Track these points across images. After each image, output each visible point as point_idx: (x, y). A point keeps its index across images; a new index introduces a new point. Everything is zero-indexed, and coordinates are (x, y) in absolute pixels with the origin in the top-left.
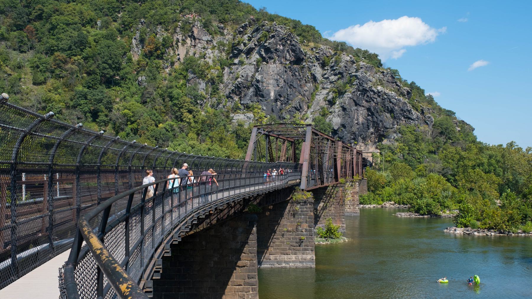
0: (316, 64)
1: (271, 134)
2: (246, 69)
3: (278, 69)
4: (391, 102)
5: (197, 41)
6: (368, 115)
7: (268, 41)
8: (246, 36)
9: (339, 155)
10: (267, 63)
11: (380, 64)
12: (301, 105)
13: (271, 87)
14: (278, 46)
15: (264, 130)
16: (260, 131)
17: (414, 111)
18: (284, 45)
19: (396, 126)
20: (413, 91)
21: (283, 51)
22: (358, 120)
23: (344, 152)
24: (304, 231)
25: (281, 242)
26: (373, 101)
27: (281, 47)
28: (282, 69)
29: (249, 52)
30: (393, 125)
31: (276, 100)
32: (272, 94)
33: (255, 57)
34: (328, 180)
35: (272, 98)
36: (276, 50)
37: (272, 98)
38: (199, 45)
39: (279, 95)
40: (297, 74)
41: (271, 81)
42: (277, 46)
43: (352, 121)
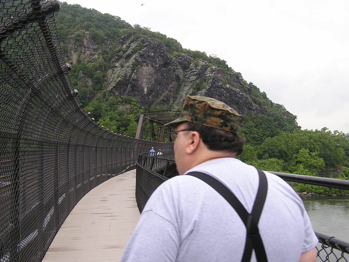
21: (153, 57)
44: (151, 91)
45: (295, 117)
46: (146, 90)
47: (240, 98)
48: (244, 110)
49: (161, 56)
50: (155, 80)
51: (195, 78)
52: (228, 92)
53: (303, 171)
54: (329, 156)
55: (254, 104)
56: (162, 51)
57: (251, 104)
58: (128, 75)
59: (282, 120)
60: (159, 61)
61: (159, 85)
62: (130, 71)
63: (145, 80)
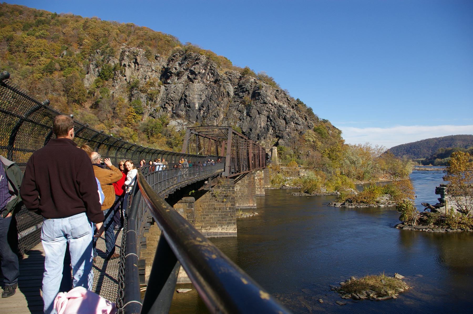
0: (229, 84)
1: (200, 134)
2: (177, 85)
3: (201, 87)
4: (284, 112)
5: (140, 66)
6: (268, 121)
7: (194, 67)
8: (177, 62)
9: (251, 151)
10: (193, 82)
11: (126, 174)
12: (219, 113)
13: (196, 101)
14: (201, 70)
15: (195, 131)
16: (192, 131)
17: (300, 119)
18: (205, 70)
19: (287, 130)
20: (297, 105)
21: (204, 74)
22: (260, 124)
23: (254, 149)
24: (228, 209)
25: (210, 218)
26: (271, 111)
27: (204, 71)
28: (204, 87)
29: (179, 75)
30: (286, 128)
31: (200, 109)
32: (197, 106)
33: (185, 78)
34: (243, 169)
35: (197, 109)
36: (199, 73)
37: (197, 109)
38: (141, 69)
39: (202, 106)
40: (215, 91)
41: (196, 96)
42: (200, 70)
43: (257, 126)
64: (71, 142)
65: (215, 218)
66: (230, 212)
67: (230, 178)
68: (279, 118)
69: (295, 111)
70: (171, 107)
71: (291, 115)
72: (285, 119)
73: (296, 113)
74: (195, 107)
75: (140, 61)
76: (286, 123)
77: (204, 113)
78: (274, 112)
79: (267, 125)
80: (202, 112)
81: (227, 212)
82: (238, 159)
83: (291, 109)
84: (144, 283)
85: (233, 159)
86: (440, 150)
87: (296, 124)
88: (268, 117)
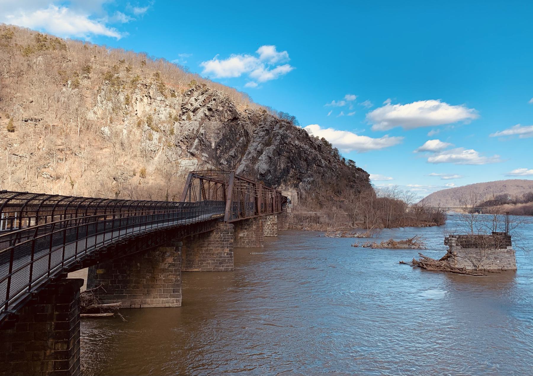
4: (305, 153)
13: (212, 140)
14: (219, 108)
17: (323, 161)
21: (222, 112)
22: (280, 166)
25: (207, 263)
27: (221, 109)
30: (307, 170)
31: (216, 149)
32: (213, 145)
38: (154, 104)
44: (218, 145)
45: (369, 175)
46: (213, 145)
47: (309, 155)
48: (313, 166)
49: (230, 111)
50: (223, 135)
51: (263, 133)
52: (297, 149)
53: (17, 241)
54: (270, 177)
55: (323, 161)
56: (231, 105)
57: (320, 161)
58: (196, 129)
59: (398, 205)
60: (228, 116)
61: (228, 140)
62: (198, 125)
63: (213, 135)
64: (331, 102)
65: (212, 264)
66: (228, 257)
67: (230, 223)
68: (300, 159)
69: (317, 153)
70: (185, 146)
71: (313, 156)
72: (306, 160)
73: (319, 156)
74: (211, 147)
75: (153, 95)
76: (308, 165)
77: (221, 152)
78: (295, 153)
79: (287, 166)
80: (218, 152)
81: (225, 257)
82: (265, 204)
83: (313, 151)
84: (82, 280)
85: (262, 204)
86: (489, 197)
87: (319, 166)
88: (289, 158)
